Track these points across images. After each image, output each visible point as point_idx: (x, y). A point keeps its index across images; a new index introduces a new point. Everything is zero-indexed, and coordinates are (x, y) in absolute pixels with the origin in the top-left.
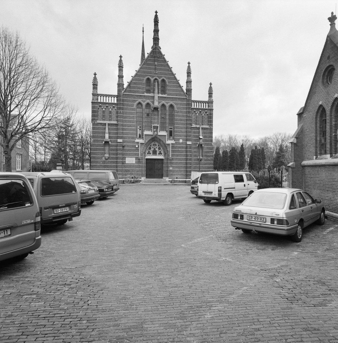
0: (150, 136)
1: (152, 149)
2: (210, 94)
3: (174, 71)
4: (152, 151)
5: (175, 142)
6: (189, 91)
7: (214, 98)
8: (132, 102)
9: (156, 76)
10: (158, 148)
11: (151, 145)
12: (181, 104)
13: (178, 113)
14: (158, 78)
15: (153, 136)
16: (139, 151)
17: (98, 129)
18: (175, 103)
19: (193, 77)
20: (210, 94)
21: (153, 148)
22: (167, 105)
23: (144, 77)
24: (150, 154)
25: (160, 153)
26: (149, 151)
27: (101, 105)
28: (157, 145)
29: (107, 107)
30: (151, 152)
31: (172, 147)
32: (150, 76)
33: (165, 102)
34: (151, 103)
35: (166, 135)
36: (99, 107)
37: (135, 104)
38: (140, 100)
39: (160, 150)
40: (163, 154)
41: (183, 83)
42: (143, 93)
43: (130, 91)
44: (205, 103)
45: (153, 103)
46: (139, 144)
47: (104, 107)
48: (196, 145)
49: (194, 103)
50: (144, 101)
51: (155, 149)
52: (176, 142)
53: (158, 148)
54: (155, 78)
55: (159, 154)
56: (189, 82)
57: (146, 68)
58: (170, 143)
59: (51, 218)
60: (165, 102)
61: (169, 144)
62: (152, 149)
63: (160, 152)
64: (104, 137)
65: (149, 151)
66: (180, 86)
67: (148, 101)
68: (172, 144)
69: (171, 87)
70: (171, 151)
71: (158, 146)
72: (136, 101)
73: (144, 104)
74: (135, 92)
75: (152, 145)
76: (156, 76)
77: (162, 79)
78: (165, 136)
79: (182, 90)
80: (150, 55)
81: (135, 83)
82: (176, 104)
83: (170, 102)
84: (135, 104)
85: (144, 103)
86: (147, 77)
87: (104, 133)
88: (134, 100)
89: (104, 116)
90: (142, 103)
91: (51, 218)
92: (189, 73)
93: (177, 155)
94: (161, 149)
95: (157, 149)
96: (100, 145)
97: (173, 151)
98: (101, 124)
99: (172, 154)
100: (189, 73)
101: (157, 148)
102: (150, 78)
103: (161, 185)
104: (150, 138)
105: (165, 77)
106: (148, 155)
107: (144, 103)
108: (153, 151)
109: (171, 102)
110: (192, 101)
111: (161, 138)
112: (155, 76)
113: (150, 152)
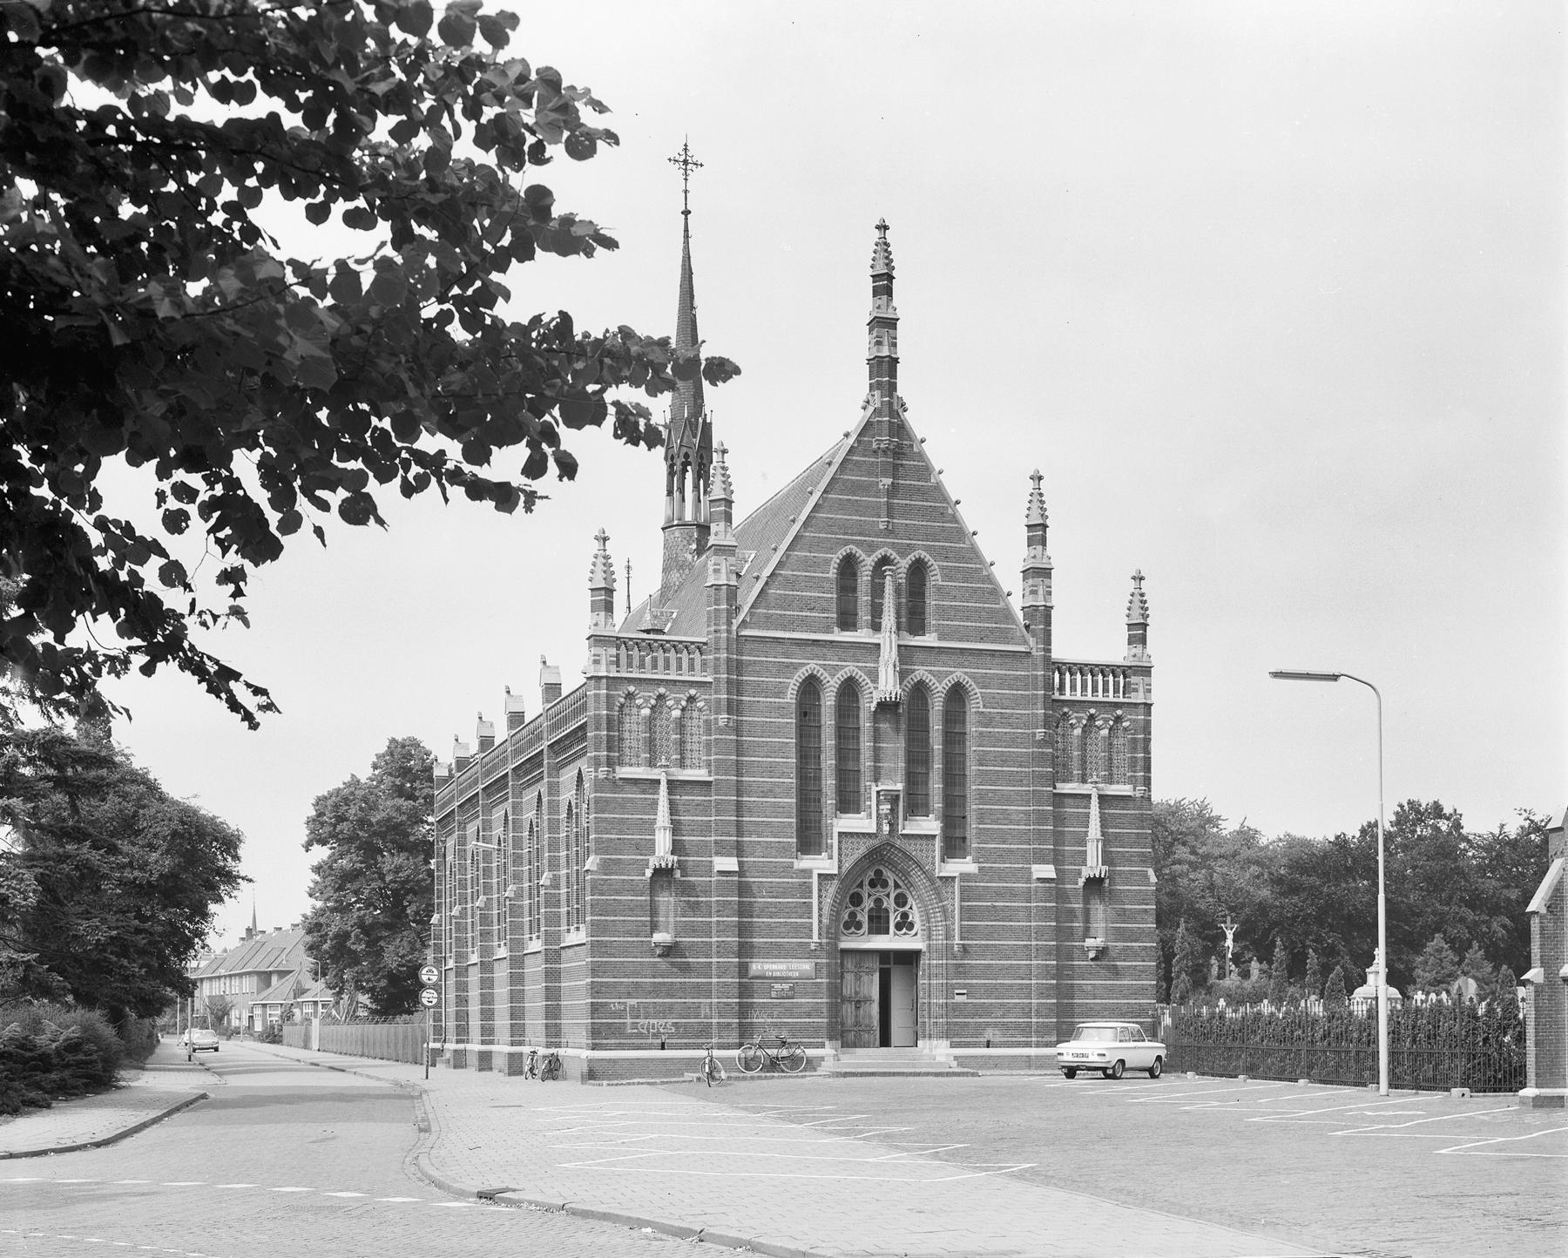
1: (868, 904)
2: (1138, 634)
3: (969, 516)
4: (866, 910)
5: (976, 865)
6: (1041, 618)
7: (1157, 648)
9: (885, 544)
10: (892, 896)
12: (1003, 682)
14: (894, 555)
15: (876, 842)
16: (811, 912)
17: (622, 806)
18: (973, 676)
19: (1057, 550)
20: (1138, 634)
21: (870, 895)
22: (939, 689)
26: (853, 915)
27: (632, 689)
28: (891, 883)
29: (660, 697)
30: (863, 918)
31: (963, 890)
32: (858, 544)
33: (966, 673)
34: (864, 677)
35: (938, 832)
36: (622, 700)
37: (793, 681)
38: (812, 666)
40: (917, 927)
41: (1009, 577)
42: (828, 630)
43: (769, 622)
44: (1102, 672)
45: (874, 675)
46: (811, 877)
47: (1106, 720)
48: (644, 874)
49: (1062, 674)
50: (833, 670)
51: (878, 901)
52: (980, 869)
53: (897, 897)
54: (879, 554)
55: (899, 927)
56: (1039, 574)
57: (842, 506)
58: (957, 874)
60: (966, 673)
61: (948, 880)
62: (868, 904)
64: (650, 848)
65: (853, 915)
66: (995, 593)
67: (850, 668)
68: (965, 877)
69: (955, 598)
71: (897, 886)
72: (796, 667)
73: (832, 682)
76: (885, 544)
77: (912, 557)
78: (934, 837)
79: (1007, 615)
80: (858, 440)
81: (790, 583)
82: (984, 682)
83: (952, 672)
84: (792, 686)
85: (940, 682)
86: (842, 552)
87: (650, 827)
88: (788, 666)
89: (651, 744)
90: (824, 675)
92: (1038, 533)
93: (991, 933)
94: (910, 900)
95: (889, 903)
96: (632, 889)
97: (967, 913)
98: (635, 782)
100: (1038, 533)
101: (888, 896)
102: (859, 553)
103: (634, 1083)
104: (862, 849)
105: (927, 549)
109: (959, 674)
110: (1054, 663)
111: (912, 848)
112: (879, 548)
113: (859, 917)
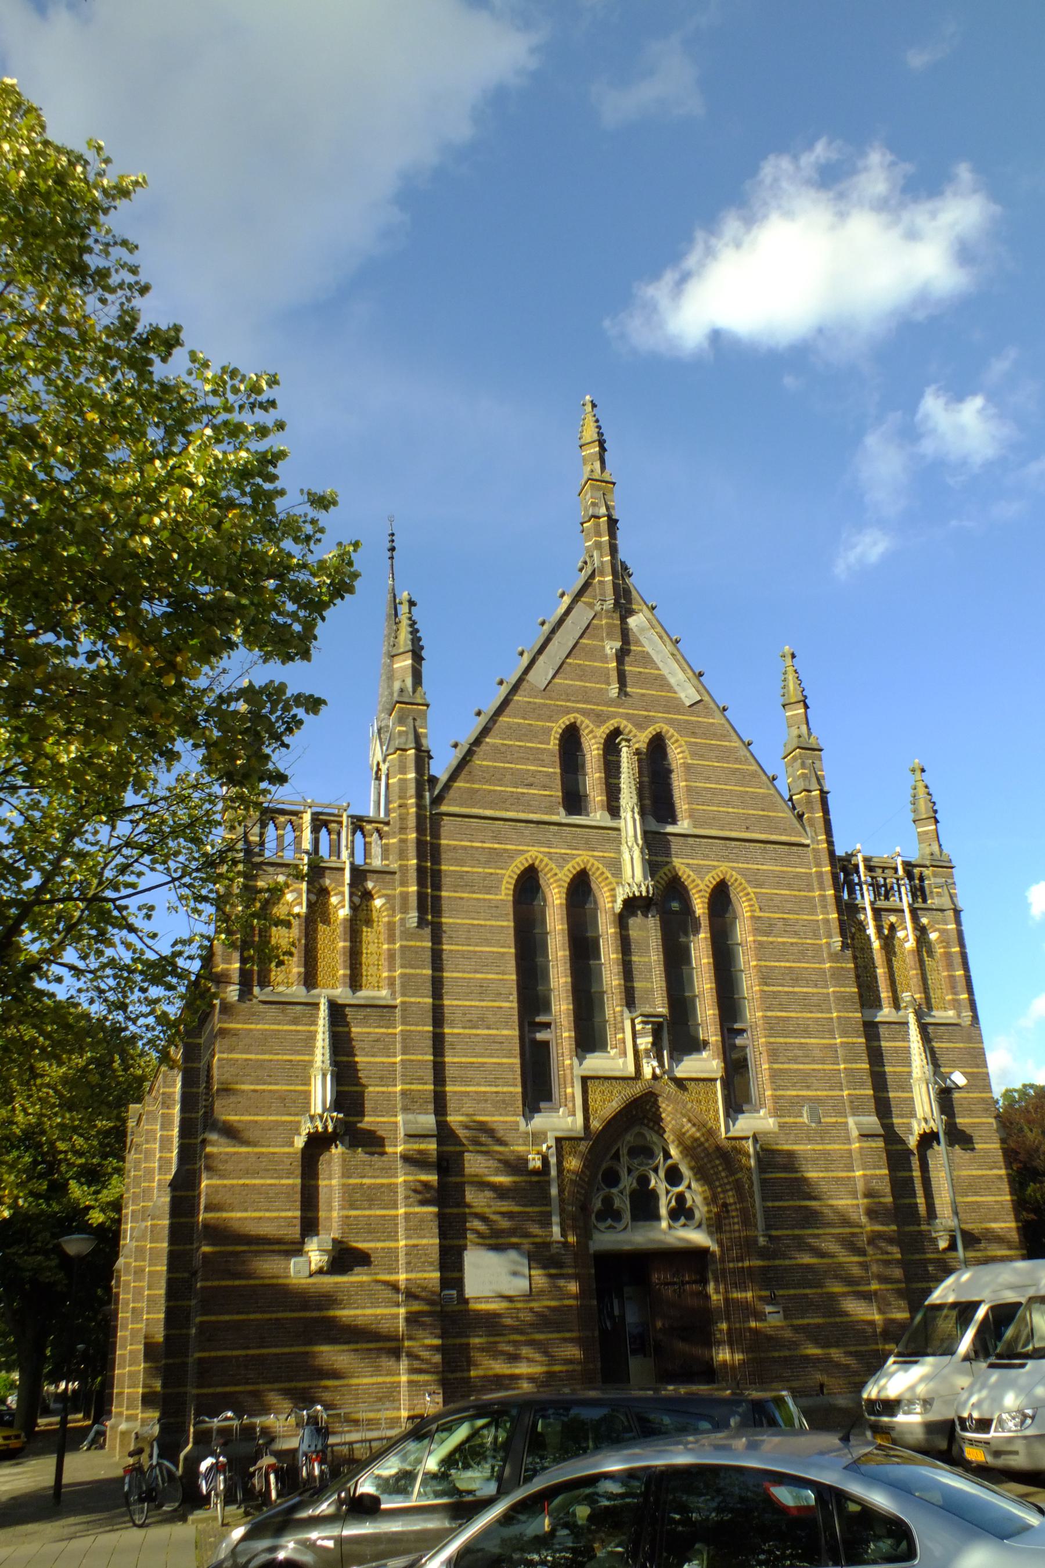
0: (618, 1087)
1: (628, 1182)
8: (487, 863)
11: (617, 1156)
13: (768, 934)
18: (742, 872)
21: (630, 1171)
23: (550, 719)
24: (617, 1216)
25: (681, 1212)
26: (608, 1201)
37: (508, 873)
39: (680, 1189)
46: (776, 1099)
52: (782, 1126)
59: (921, 1200)
60: (688, 865)
63: (681, 1198)
69: (708, 779)
70: (756, 1188)
72: (512, 855)
74: (502, 801)
75: (624, 1151)
83: (715, 867)
84: (506, 879)
91: (921, 1200)
99: (766, 1210)
106: (602, 1226)
107: (561, 867)
108: (633, 1195)
109: (723, 869)
113: (617, 1203)
